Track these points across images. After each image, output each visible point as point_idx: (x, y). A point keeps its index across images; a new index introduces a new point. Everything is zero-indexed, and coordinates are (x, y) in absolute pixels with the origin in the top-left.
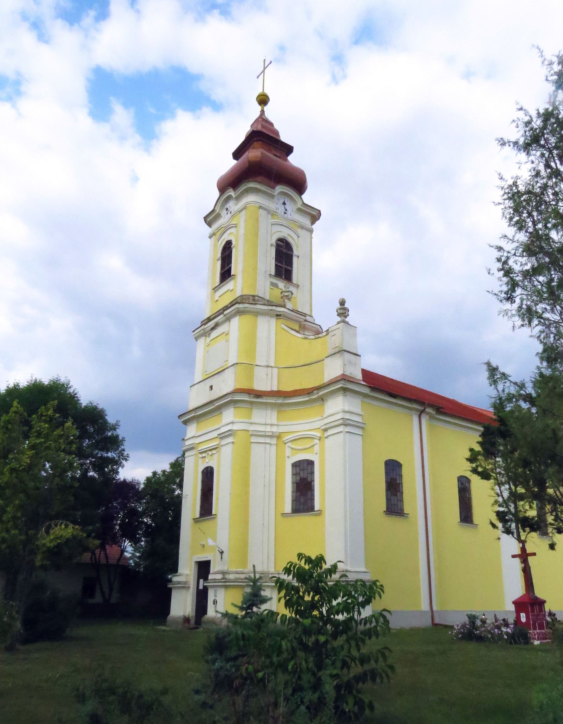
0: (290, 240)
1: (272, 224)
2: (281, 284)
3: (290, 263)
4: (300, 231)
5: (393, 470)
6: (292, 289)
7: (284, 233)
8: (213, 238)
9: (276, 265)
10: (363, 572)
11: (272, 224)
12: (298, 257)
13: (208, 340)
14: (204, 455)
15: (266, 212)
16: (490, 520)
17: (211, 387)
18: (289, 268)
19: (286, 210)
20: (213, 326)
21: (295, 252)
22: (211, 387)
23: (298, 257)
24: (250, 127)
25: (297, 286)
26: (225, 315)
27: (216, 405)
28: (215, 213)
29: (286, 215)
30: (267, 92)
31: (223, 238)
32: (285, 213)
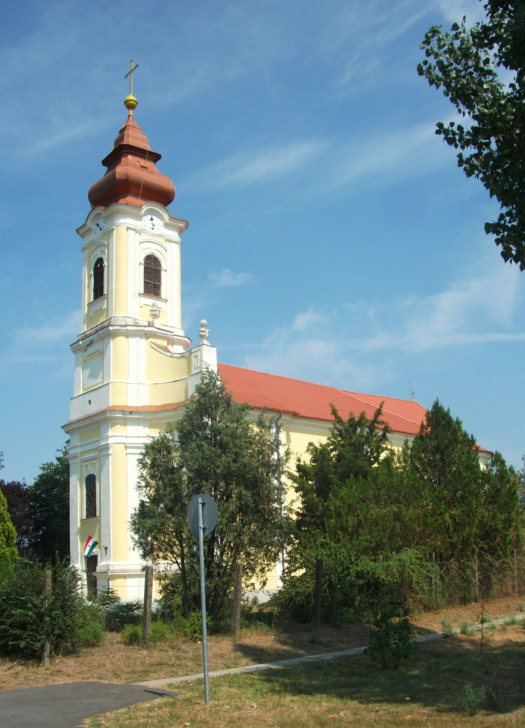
0: (158, 255)
1: (140, 243)
2: (150, 301)
3: (159, 279)
4: (167, 245)
5: (162, 636)
6: (159, 304)
7: (153, 250)
8: (87, 252)
9: (145, 282)
10: (151, 692)
11: (140, 243)
12: (166, 271)
13: (85, 354)
14: (86, 463)
15: (134, 232)
16: (332, 405)
17: (90, 402)
18: (157, 283)
19: (154, 225)
20: (89, 343)
21: (164, 266)
22: (90, 402)
23: (166, 271)
24: (119, 133)
25: (166, 301)
26: (99, 335)
27: (95, 420)
28: (86, 228)
29: (153, 231)
30: (88, 206)
31: (94, 254)
32: (153, 229)
